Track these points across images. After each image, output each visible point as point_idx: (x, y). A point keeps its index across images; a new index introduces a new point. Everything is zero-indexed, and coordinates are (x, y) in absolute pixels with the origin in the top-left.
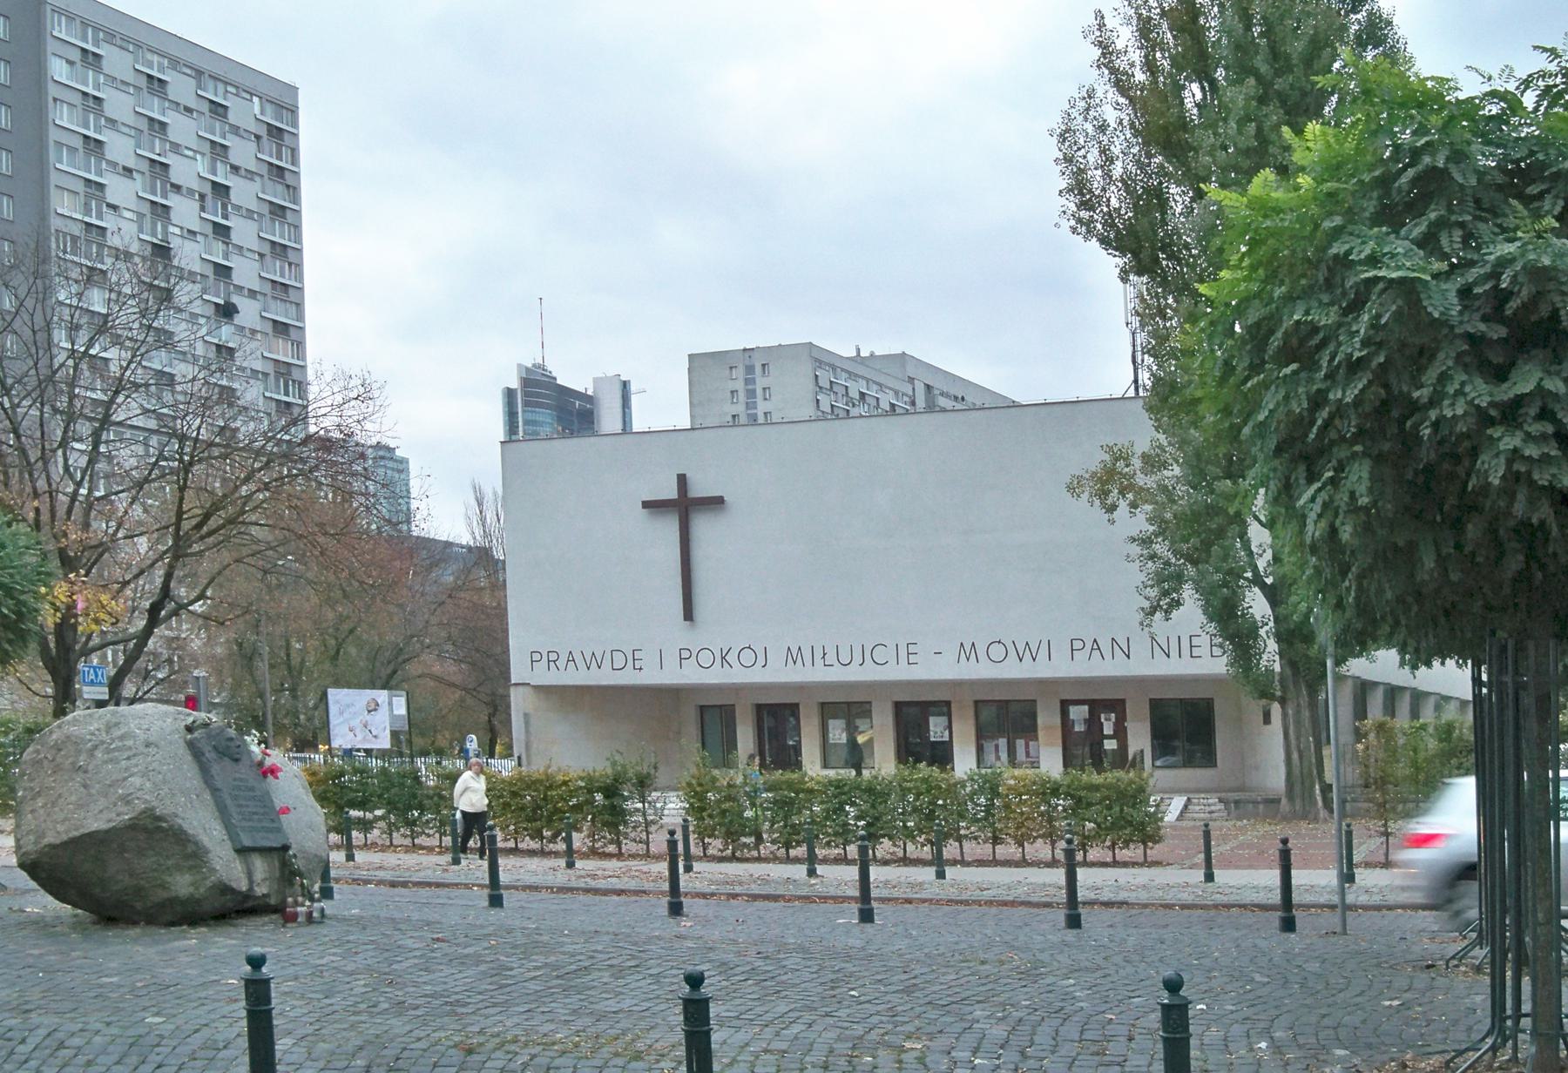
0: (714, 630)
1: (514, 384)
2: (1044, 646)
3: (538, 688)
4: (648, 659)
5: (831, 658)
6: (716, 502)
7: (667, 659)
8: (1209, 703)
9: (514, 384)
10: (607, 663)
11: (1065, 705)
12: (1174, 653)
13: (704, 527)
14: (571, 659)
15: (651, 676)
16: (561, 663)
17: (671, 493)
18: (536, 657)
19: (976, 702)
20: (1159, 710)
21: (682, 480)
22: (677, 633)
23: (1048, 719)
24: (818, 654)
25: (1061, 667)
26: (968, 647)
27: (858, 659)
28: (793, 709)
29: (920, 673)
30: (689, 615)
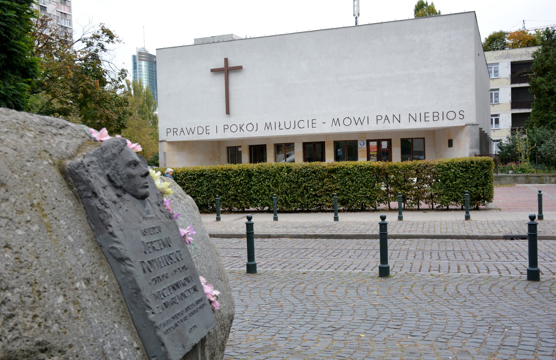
0: (236, 119)
1: (135, 54)
2: (366, 119)
3: (169, 142)
4: (212, 130)
5: (282, 126)
6: (239, 68)
7: (220, 129)
8: (265, 146)
9: (135, 54)
10: (196, 132)
11: (368, 142)
12: (418, 119)
13: (234, 78)
14: (182, 131)
15: (213, 136)
16: (178, 133)
17: (222, 65)
18: (169, 131)
19: (424, 138)
20: (337, 145)
21: (226, 60)
22: (224, 120)
23: (362, 148)
24: (277, 125)
25: (373, 126)
26: (336, 120)
27: (293, 126)
28: (322, 144)
29: (317, 131)
30: (228, 112)
